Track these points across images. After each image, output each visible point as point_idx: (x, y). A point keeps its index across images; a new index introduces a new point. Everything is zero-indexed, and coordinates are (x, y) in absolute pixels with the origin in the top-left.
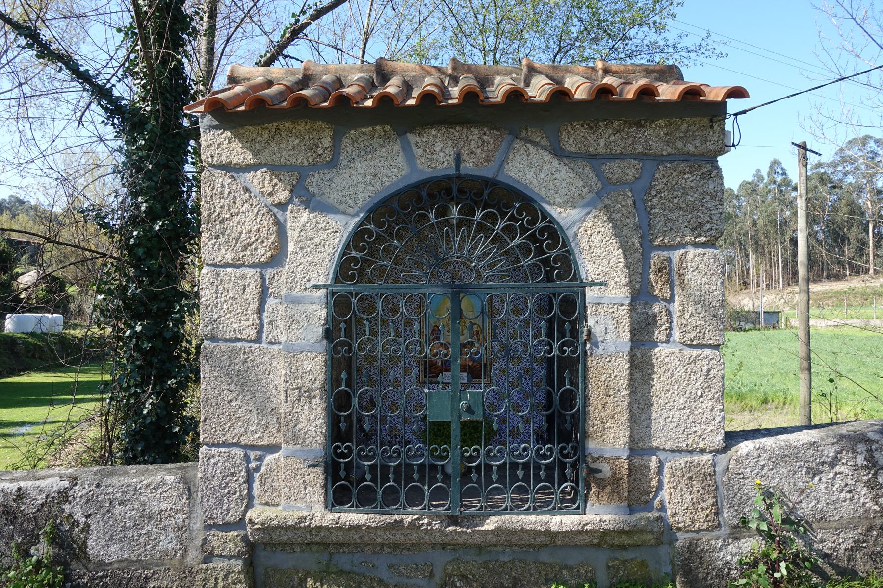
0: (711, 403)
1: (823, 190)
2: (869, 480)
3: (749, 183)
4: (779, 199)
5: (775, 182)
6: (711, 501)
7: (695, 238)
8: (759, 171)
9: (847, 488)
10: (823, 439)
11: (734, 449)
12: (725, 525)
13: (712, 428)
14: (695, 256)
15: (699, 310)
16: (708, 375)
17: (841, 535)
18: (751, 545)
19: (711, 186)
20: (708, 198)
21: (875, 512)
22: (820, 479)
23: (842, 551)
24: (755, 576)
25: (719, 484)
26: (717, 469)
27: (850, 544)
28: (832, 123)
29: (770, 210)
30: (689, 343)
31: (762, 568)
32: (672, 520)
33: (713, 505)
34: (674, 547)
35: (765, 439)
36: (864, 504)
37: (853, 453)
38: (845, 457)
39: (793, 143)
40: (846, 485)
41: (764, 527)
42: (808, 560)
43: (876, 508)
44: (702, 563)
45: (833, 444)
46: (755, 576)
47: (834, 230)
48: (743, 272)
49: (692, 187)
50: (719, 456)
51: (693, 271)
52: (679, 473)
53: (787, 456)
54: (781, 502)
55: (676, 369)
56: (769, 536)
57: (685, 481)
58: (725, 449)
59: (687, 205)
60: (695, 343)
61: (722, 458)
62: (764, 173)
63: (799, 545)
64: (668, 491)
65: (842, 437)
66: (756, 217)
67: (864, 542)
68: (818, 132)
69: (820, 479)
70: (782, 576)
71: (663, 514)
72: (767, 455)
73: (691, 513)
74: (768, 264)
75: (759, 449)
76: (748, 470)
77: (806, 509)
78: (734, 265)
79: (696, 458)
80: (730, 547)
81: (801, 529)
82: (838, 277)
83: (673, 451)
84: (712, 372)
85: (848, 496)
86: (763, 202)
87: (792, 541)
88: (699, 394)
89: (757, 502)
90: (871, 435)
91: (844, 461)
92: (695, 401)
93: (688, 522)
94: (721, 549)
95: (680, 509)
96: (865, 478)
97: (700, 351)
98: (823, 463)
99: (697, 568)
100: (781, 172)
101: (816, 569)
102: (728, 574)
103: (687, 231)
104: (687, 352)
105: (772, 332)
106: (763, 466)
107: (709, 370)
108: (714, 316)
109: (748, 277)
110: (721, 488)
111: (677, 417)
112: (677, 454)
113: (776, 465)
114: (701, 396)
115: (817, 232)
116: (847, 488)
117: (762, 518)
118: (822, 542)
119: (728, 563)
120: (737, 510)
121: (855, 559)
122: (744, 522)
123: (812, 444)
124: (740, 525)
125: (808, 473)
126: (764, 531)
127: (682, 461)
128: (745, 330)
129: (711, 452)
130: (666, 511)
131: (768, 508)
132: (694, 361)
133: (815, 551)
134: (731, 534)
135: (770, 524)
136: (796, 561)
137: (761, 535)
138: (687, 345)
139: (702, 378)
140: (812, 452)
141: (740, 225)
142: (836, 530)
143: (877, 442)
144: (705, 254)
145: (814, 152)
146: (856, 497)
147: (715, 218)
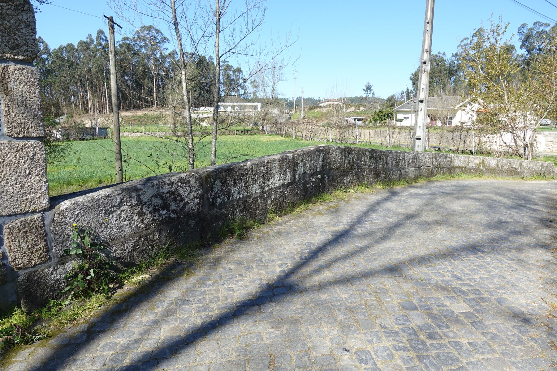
0: (37, 178)
1: (129, 55)
2: (139, 212)
3: (85, 43)
4: (104, 56)
5: (101, 45)
6: (42, 244)
7: (15, 55)
8: (90, 35)
9: (128, 218)
10: (113, 192)
11: (57, 207)
12: (54, 257)
13: (39, 195)
14: (15, 70)
15: (23, 111)
16: (33, 159)
17: (126, 245)
18: (72, 265)
19: (25, 17)
20: (23, 26)
21: (143, 228)
22: (113, 216)
23: (126, 254)
24: (76, 283)
25: (48, 231)
26: (45, 222)
27: (131, 248)
28: (126, 7)
29: (99, 62)
30: (16, 135)
31: (80, 276)
32: (13, 264)
33: (44, 246)
34: (17, 282)
35: (78, 197)
36: (137, 225)
37: (130, 198)
38: (126, 201)
39: (105, 16)
40: (127, 216)
41: (80, 252)
42: (107, 263)
43: (143, 226)
44: (39, 286)
45: (119, 194)
46: (76, 283)
47: (136, 80)
48: (84, 102)
49: (8, 14)
50: (47, 213)
51: (14, 81)
52: (16, 230)
53: (93, 206)
54: (90, 234)
55: (7, 155)
56: (83, 256)
57: (21, 234)
58: (51, 208)
59: (5, 28)
60: (21, 135)
61: (49, 215)
62: (94, 37)
63: (102, 256)
64: (8, 245)
65: (123, 190)
66: (90, 66)
67: (138, 245)
68: (119, 12)
69: (113, 216)
70: (91, 277)
71: (5, 262)
72: (80, 207)
73: (28, 255)
74: (100, 98)
75: (74, 204)
76: (68, 219)
77: (105, 235)
78: (78, 97)
79: (29, 218)
80: (58, 271)
81: (102, 247)
82: (139, 108)
83: (10, 216)
84: (36, 156)
85: (128, 222)
86: (94, 57)
87: (98, 255)
88: (28, 172)
89: (74, 237)
90: (139, 186)
91: (125, 203)
92: (25, 178)
93: (26, 262)
94: (52, 273)
95: (19, 255)
96: (137, 211)
97: (26, 142)
98: (114, 206)
99: (36, 290)
100: (104, 39)
101: (112, 267)
102: (59, 287)
103: (7, 49)
104: (15, 142)
105: (103, 140)
106: (78, 215)
107: (34, 155)
108: (35, 116)
109: (87, 106)
110: (49, 234)
111: (11, 190)
112: (13, 217)
113: (86, 212)
114: (30, 174)
115: (127, 80)
116: (128, 218)
117: (78, 246)
118: (115, 252)
119: (58, 280)
120: (61, 246)
121: (133, 256)
122: (67, 252)
123: (107, 196)
124: (65, 254)
125: (105, 214)
126: (80, 254)
127: (18, 221)
128: (87, 140)
129: (40, 212)
130: (7, 259)
131: (82, 240)
132: (22, 149)
133: (112, 257)
134: (58, 262)
135: (83, 249)
136: (100, 266)
137: (79, 257)
138: (14, 138)
139: (29, 161)
140: (107, 201)
141: (80, 70)
142: (123, 242)
143: (142, 190)
144: (23, 69)
145: (118, 25)
146: (133, 222)
147: (30, 43)
